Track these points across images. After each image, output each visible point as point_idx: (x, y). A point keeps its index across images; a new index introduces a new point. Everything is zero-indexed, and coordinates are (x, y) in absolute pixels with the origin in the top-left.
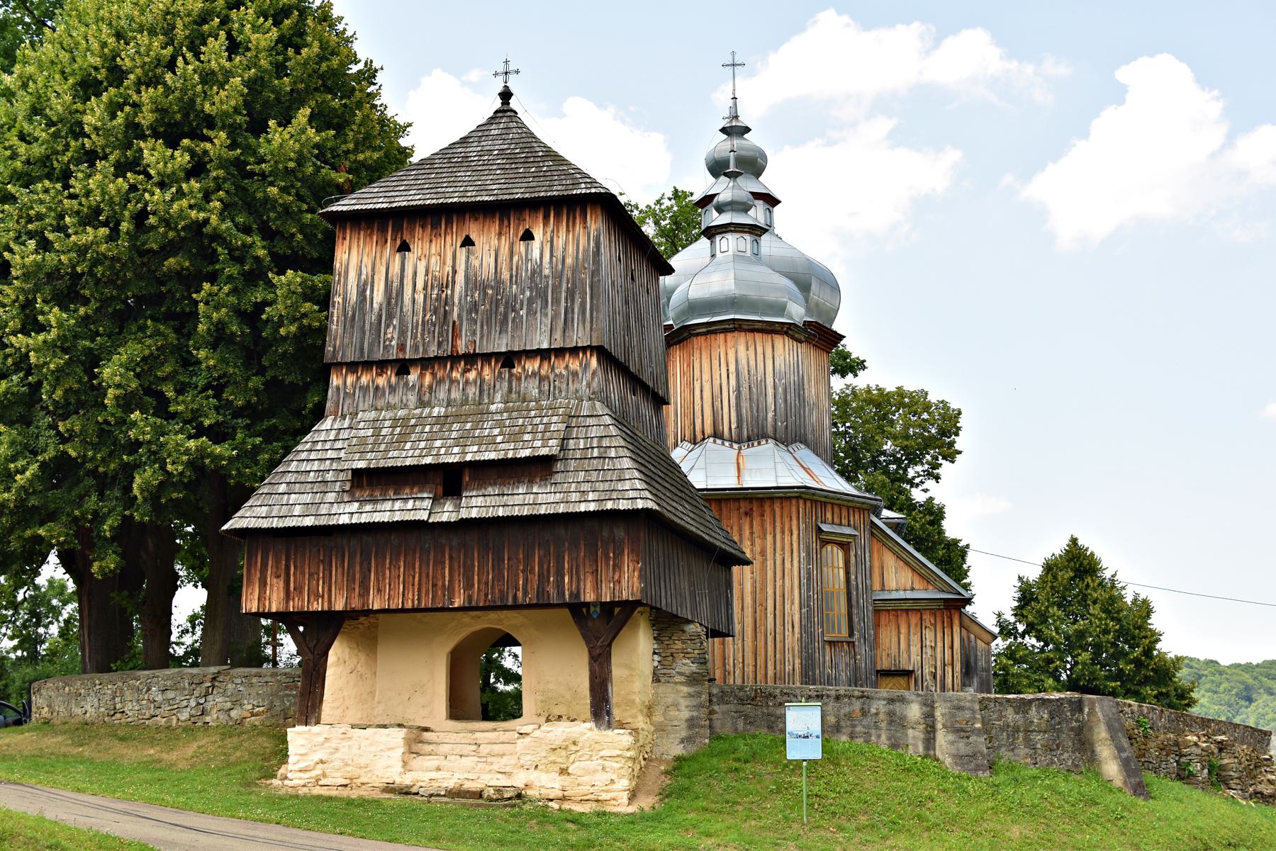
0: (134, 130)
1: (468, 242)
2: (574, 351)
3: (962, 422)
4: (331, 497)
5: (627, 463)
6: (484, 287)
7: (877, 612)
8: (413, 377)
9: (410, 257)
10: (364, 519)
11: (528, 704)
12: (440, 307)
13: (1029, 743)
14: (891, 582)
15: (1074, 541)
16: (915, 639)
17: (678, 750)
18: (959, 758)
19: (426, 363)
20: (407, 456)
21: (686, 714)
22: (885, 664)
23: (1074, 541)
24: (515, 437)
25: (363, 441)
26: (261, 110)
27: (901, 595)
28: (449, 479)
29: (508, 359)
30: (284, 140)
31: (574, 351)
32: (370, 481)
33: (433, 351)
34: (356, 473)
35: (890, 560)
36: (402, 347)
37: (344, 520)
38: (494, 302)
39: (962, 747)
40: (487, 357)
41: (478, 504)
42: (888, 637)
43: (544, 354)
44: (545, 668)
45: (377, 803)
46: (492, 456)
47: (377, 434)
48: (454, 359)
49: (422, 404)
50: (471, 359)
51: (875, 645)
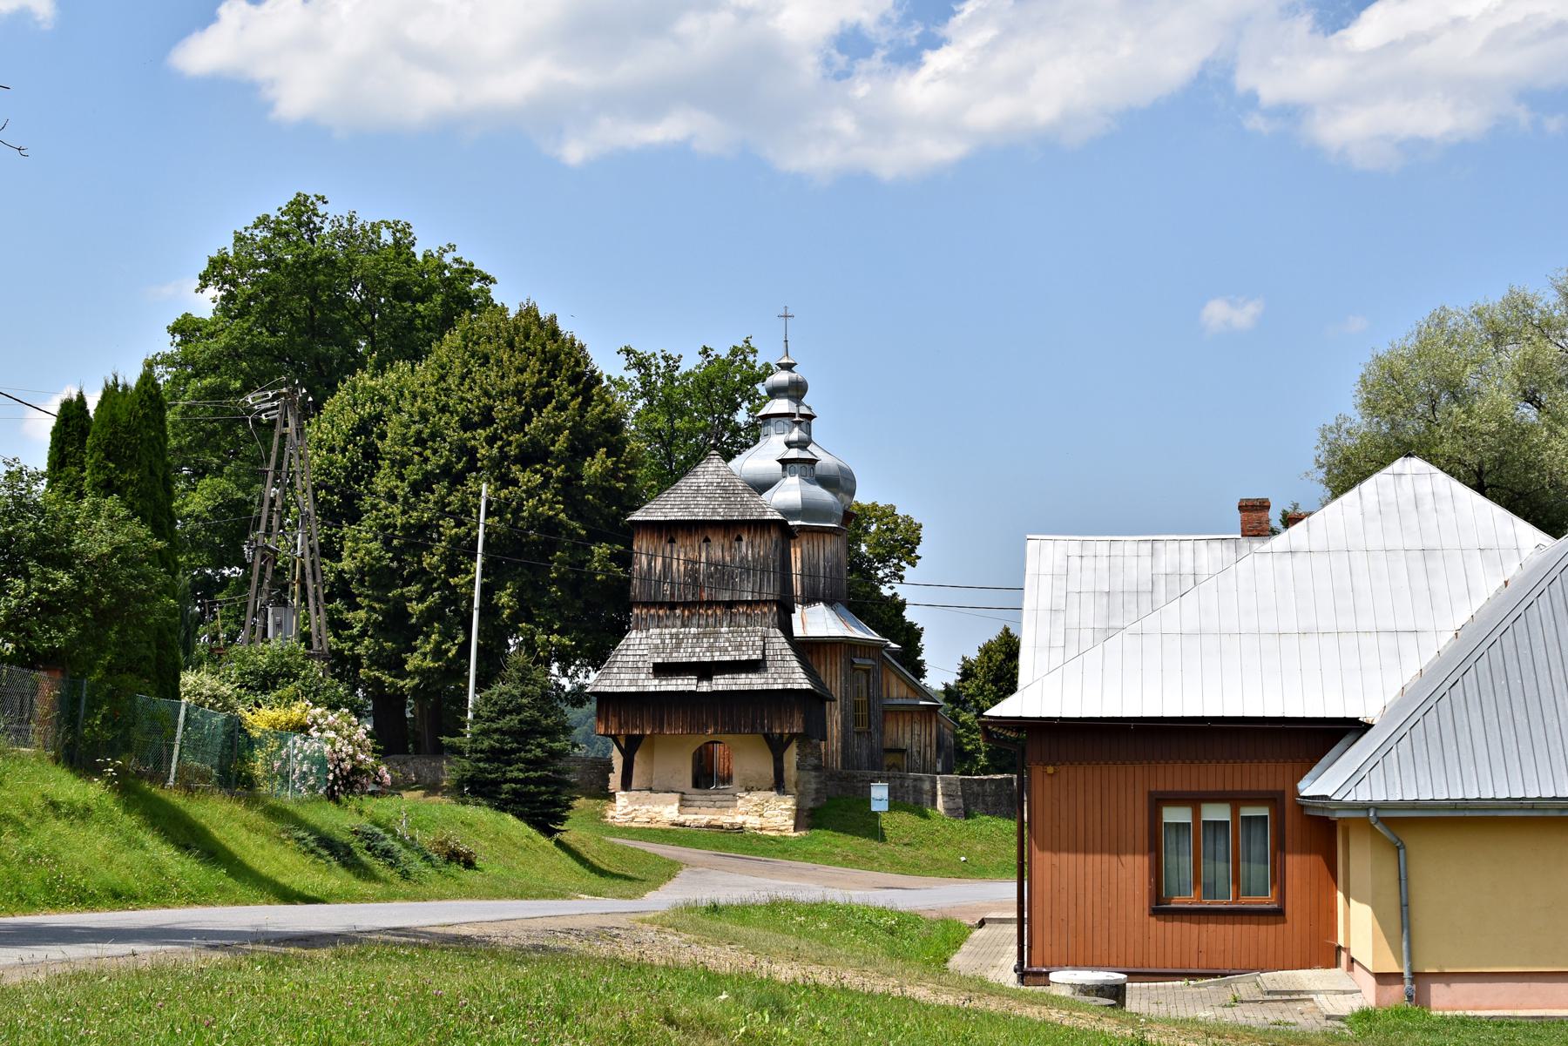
0: (504, 456)
1: (707, 540)
2: (765, 602)
3: (923, 533)
4: (643, 676)
5: (796, 664)
6: (716, 565)
7: (885, 712)
8: (678, 612)
9: (676, 546)
10: (663, 689)
11: (736, 780)
12: (693, 574)
13: (984, 802)
14: (894, 692)
15: (1007, 630)
16: (908, 729)
17: (811, 805)
18: (948, 810)
19: (686, 605)
20: (682, 656)
21: (814, 786)
22: (888, 745)
23: (1007, 630)
24: (738, 648)
25: (656, 647)
26: (582, 447)
27: (900, 701)
28: (705, 670)
29: (730, 605)
30: (594, 467)
31: (765, 602)
32: (662, 670)
33: (690, 598)
34: (656, 665)
35: (893, 680)
36: (672, 595)
37: (652, 689)
38: (722, 575)
39: (951, 805)
40: (718, 603)
41: (721, 683)
42: (890, 727)
43: (748, 603)
44: (747, 759)
45: (669, 831)
46: (727, 658)
47: (663, 642)
48: (701, 604)
49: (684, 626)
50: (710, 604)
51: (883, 733)
